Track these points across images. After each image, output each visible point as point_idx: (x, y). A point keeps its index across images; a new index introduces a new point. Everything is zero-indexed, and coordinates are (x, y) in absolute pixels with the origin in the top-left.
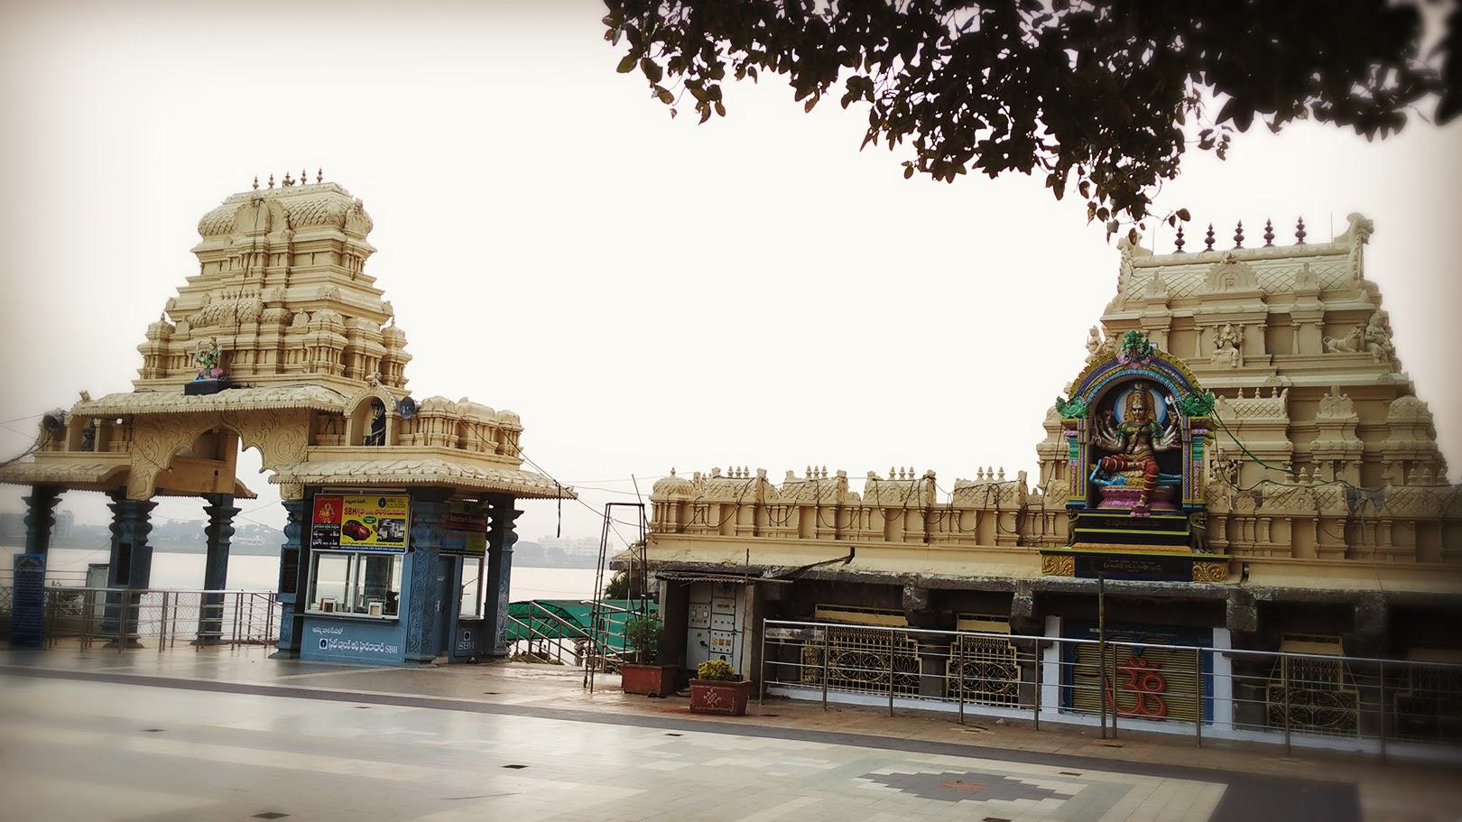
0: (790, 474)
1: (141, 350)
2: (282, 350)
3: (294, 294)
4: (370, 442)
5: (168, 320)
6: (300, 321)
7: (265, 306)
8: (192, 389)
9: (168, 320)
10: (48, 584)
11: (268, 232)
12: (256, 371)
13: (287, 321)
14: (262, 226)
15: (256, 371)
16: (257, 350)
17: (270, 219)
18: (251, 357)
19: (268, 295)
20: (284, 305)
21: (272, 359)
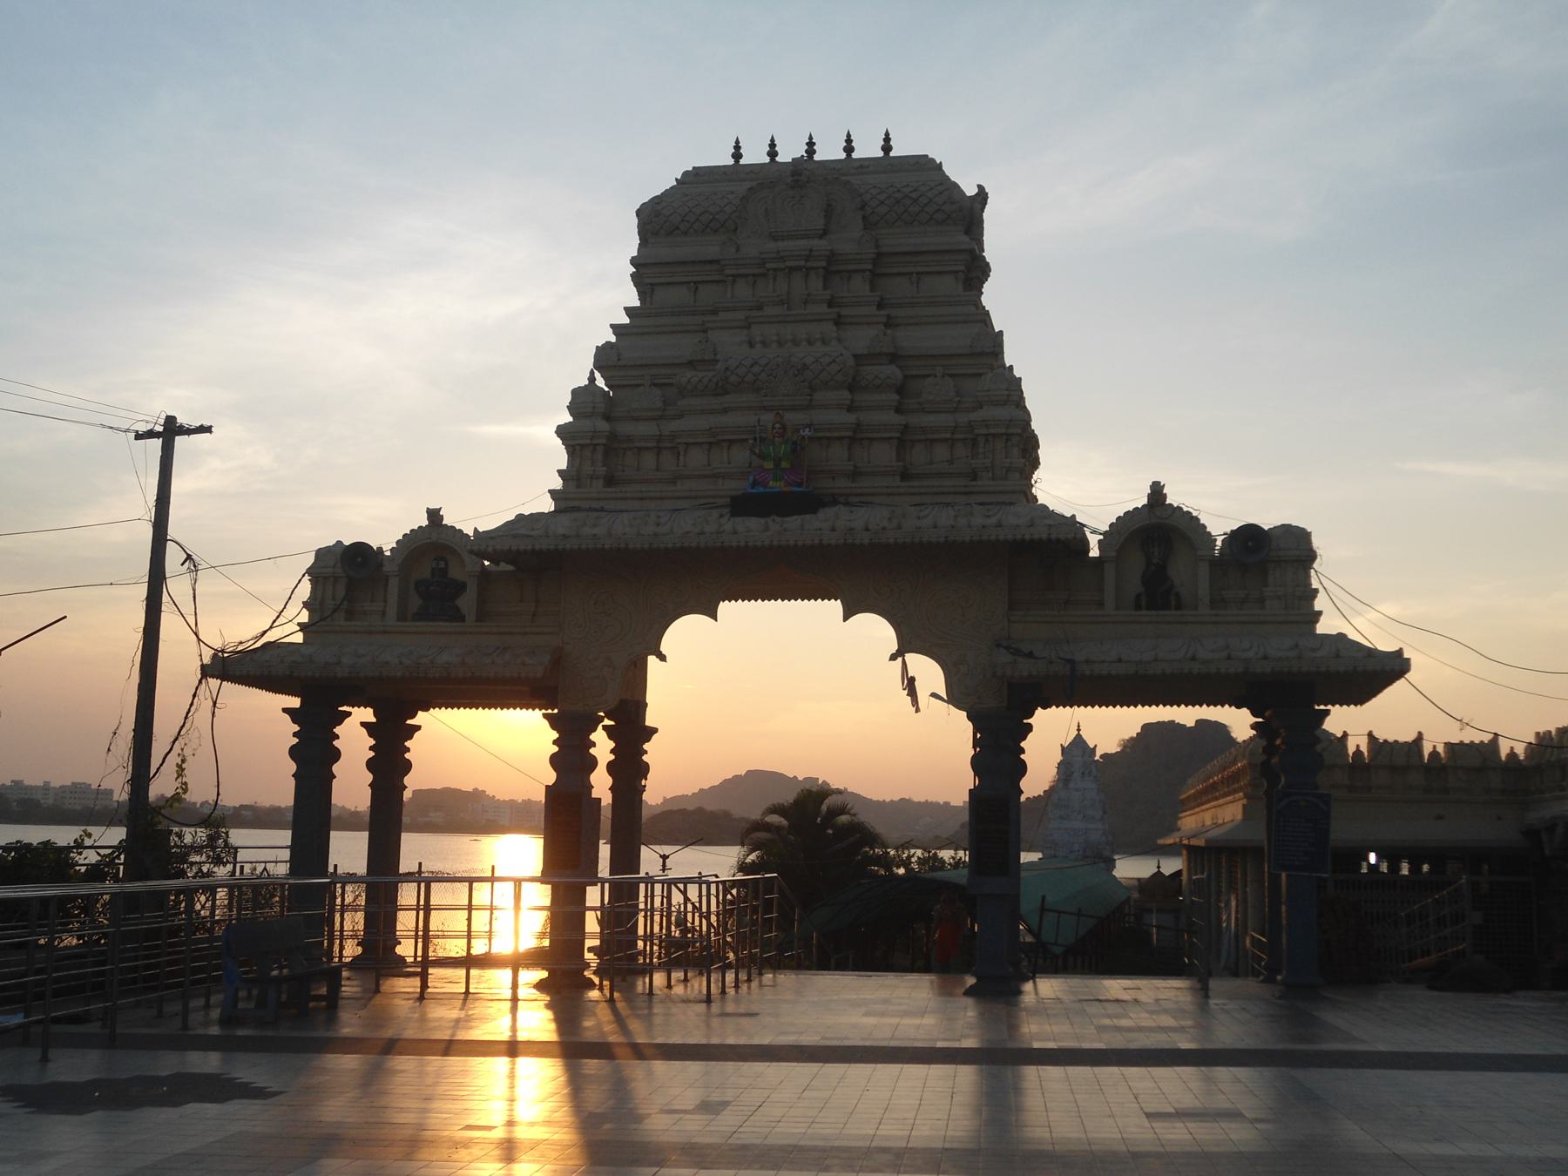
1: (562, 431)
3: (914, 339)
4: (421, 616)
5: (600, 382)
8: (741, 506)
17: (828, 211)
19: (861, 339)
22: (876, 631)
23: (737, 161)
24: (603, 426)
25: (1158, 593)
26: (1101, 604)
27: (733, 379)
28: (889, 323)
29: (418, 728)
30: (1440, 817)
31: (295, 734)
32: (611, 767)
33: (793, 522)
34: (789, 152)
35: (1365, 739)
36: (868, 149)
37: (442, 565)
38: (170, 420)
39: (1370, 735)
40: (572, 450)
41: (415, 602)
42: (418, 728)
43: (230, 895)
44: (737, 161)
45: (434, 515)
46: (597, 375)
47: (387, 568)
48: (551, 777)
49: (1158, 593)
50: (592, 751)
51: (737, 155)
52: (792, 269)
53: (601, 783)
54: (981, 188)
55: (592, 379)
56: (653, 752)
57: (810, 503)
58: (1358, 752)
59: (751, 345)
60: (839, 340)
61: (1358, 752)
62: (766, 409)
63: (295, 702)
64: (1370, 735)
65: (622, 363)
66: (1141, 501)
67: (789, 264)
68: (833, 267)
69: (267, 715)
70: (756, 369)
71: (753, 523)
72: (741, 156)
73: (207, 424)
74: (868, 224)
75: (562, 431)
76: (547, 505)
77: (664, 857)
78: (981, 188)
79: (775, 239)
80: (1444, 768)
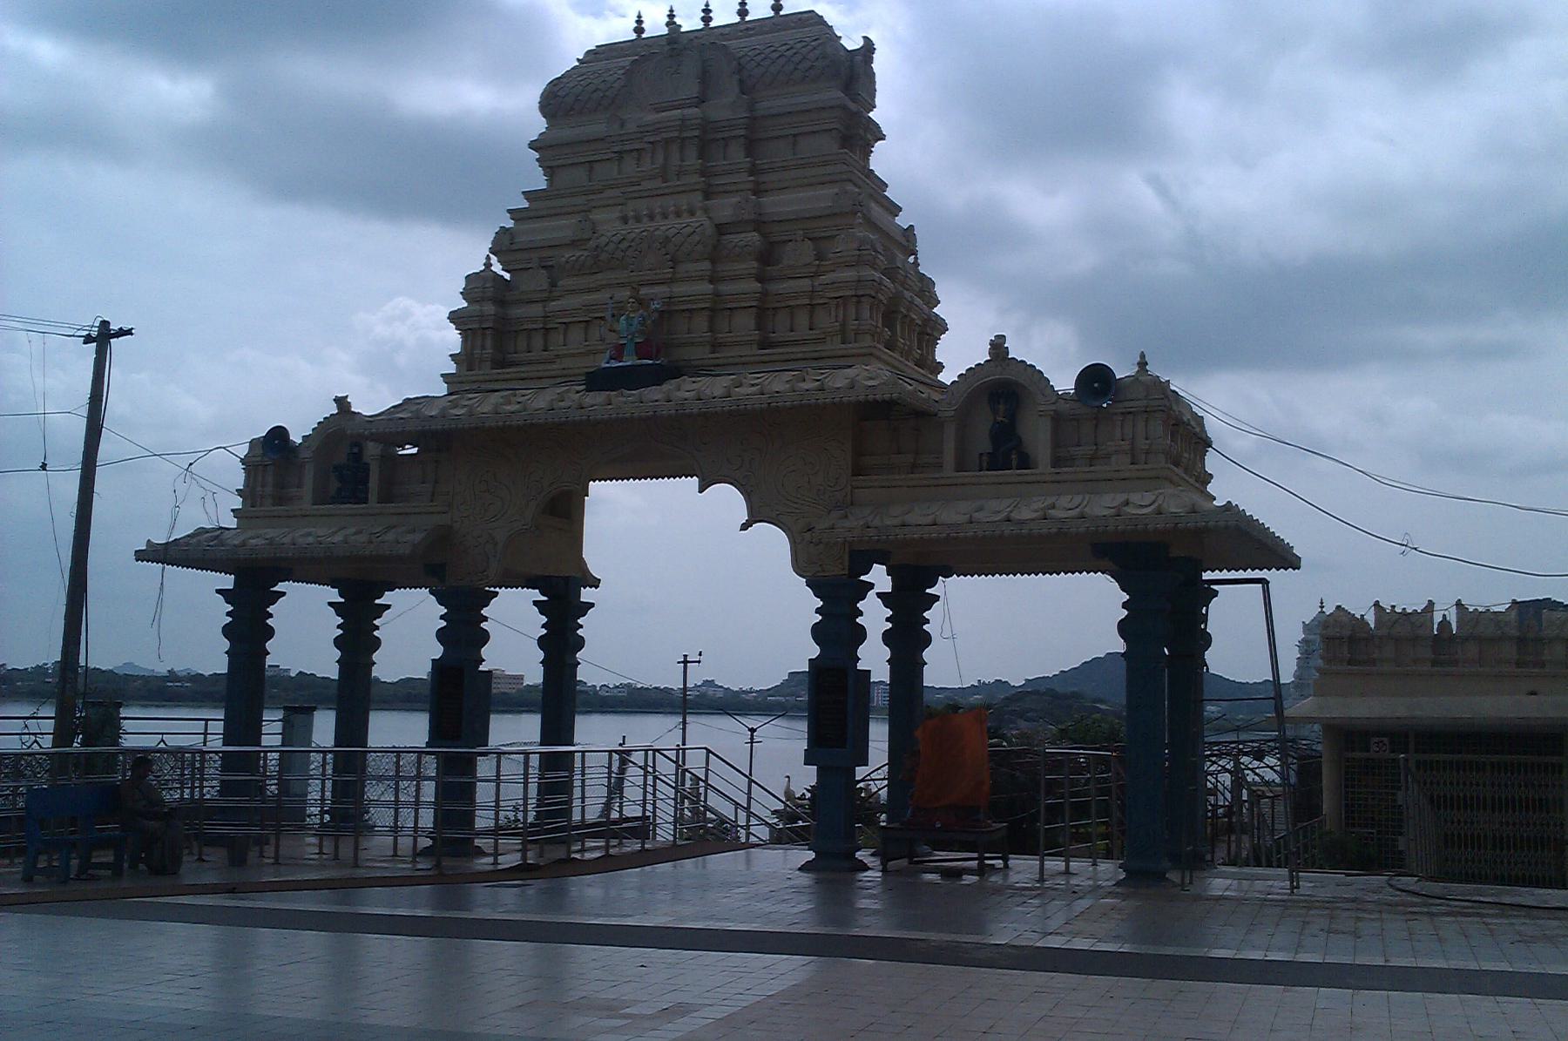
0: (595, 583)
1: (454, 317)
2: (764, 311)
3: (782, 204)
4: (339, 499)
5: (497, 268)
6: (798, 254)
7: (721, 229)
8: (597, 381)
9: (497, 268)
10: (803, 726)
11: (701, 101)
12: (715, 346)
13: (767, 257)
14: (691, 89)
15: (715, 346)
16: (718, 309)
17: (705, 78)
18: (701, 322)
19: (725, 208)
20: (759, 224)
21: (744, 323)
22: (728, 500)
23: (707, 25)
24: (489, 308)
25: (1007, 451)
26: (940, 466)
27: (604, 256)
28: (757, 192)
29: (937, 598)
30: (1533, 693)
31: (818, 611)
32: (887, 637)
33: (654, 393)
34: (656, 26)
35: (1454, 610)
36: (724, 16)
37: (356, 450)
38: (105, 324)
39: (1459, 604)
40: (466, 333)
41: (334, 485)
42: (937, 598)
43: (335, 760)
44: (707, 25)
45: (342, 402)
46: (494, 259)
47: (306, 454)
48: (437, 651)
49: (1007, 451)
50: (269, 621)
51: (707, 19)
52: (668, 142)
53: (874, 658)
54: (865, 38)
55: (488, 265)
56: (588, 626)
57: (659, 376)
58: (1445, 623)
59: (625, 220)
60: (706, 210)
61: (1445, 623)
62: (622, 285)
63: (228, 582)
64: (1459, 604)
65: (515, 247)
66: (983, 356)
67: (664, 135)
68: (707, 139)
69: (203, 596)
70: (625, 244)
71: (597, 398)
72: (711, 19)
73: (126, 327)
74: (745, 88)
75: (454, 317)
76: (441, 389)
77: (752, 730)
78: (865, 38)
79: (658, 111)
80: (1452, 638)
